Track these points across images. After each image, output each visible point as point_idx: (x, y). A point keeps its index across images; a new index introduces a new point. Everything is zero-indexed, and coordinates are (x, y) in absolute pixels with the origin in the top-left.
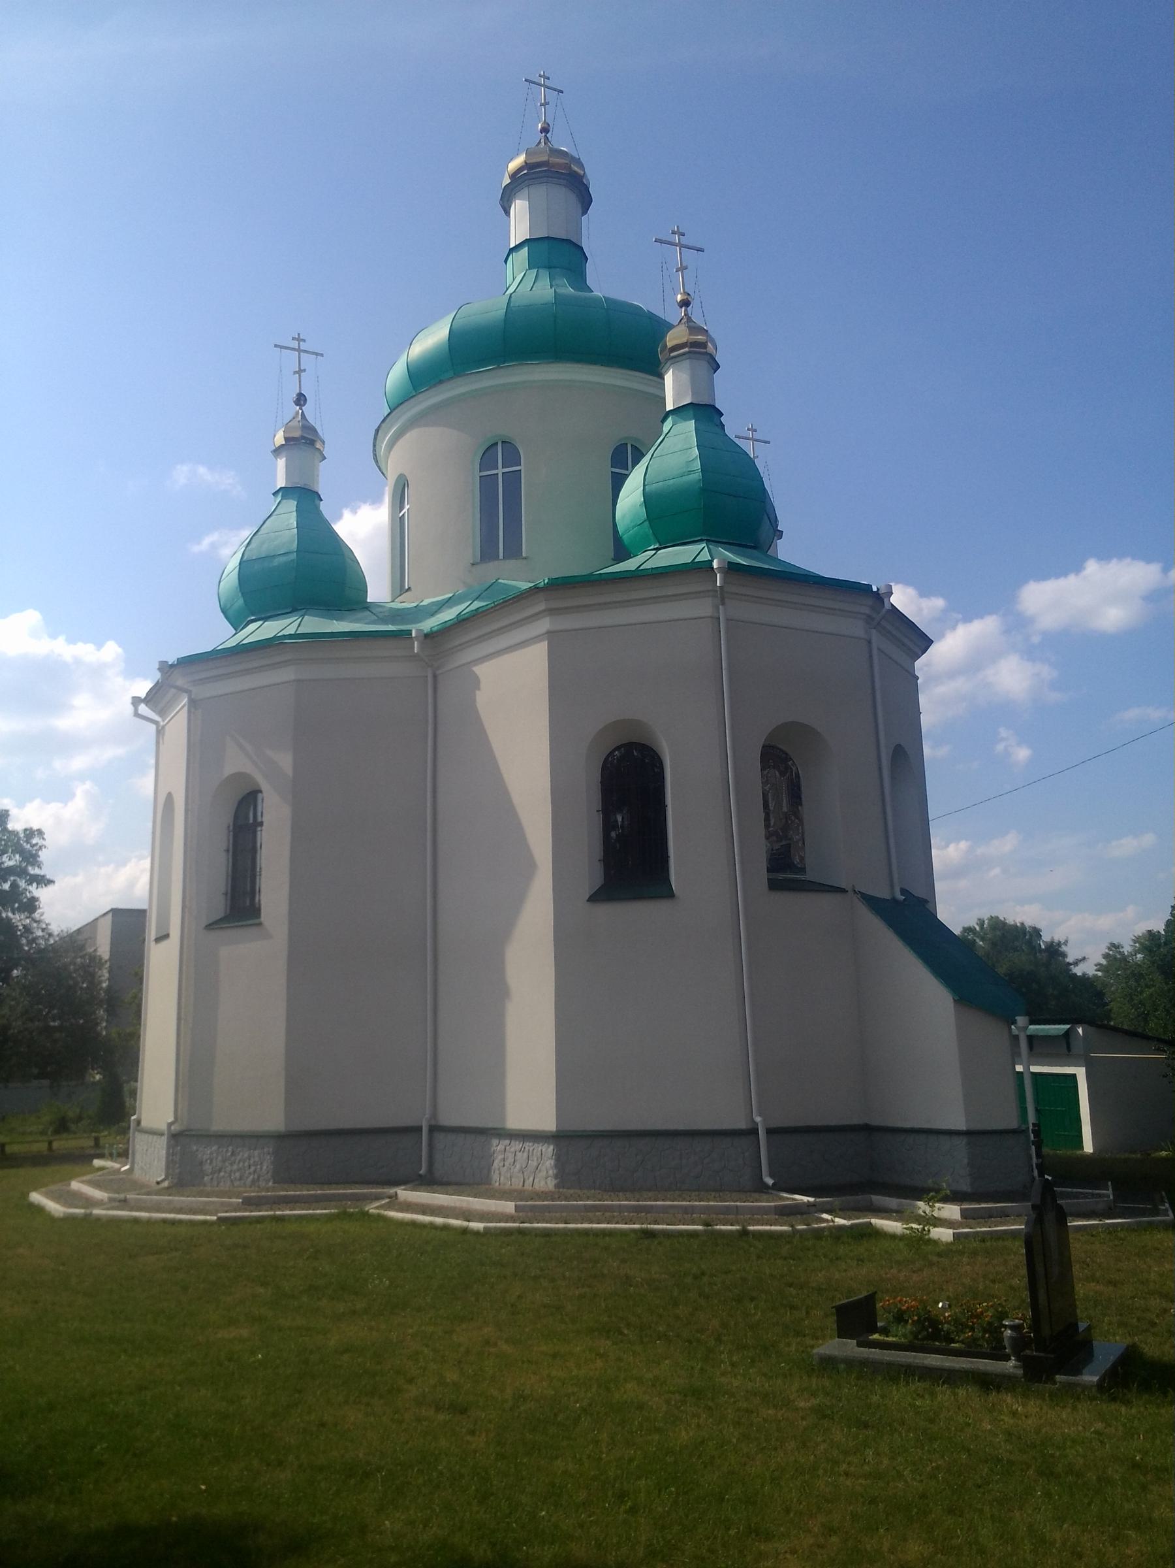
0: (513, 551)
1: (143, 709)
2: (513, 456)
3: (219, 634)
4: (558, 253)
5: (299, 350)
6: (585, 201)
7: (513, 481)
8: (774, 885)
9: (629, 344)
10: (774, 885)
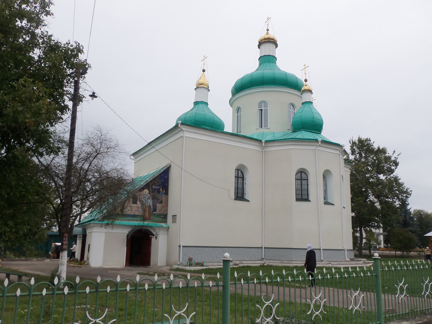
0: (266, 126)
1: (132, 157)
4: (267, 60)
8: (297, 200)
9: (292, 84)
10: (297, 200)
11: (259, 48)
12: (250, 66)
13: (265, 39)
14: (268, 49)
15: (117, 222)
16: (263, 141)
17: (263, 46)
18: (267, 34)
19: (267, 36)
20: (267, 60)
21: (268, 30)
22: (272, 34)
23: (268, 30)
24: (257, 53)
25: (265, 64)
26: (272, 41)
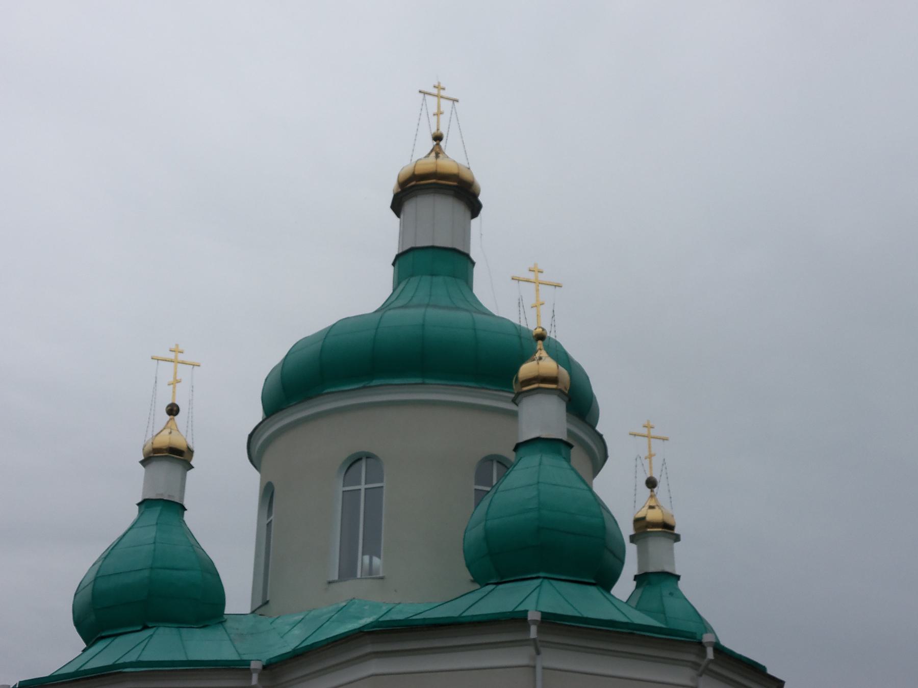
2: (376, 475)
3: (65, 649)
4: (435, 264)
5: (438, 96)
6: (475, 208)
7: (375, 496)
11: (397, 206)
12: (349, 277)
13: (435, 175)
14: (436, 218)
15: (326, 391)
16: (255, 665)
17: (417, 206)
18: (437, 152)
19: (430, 164)
20: (435, 264)
21: (438, 138)
22: (457, 157)
23: (438, 138)
24: (387, 234)
25: (414, 281)
26: (464, 193)
